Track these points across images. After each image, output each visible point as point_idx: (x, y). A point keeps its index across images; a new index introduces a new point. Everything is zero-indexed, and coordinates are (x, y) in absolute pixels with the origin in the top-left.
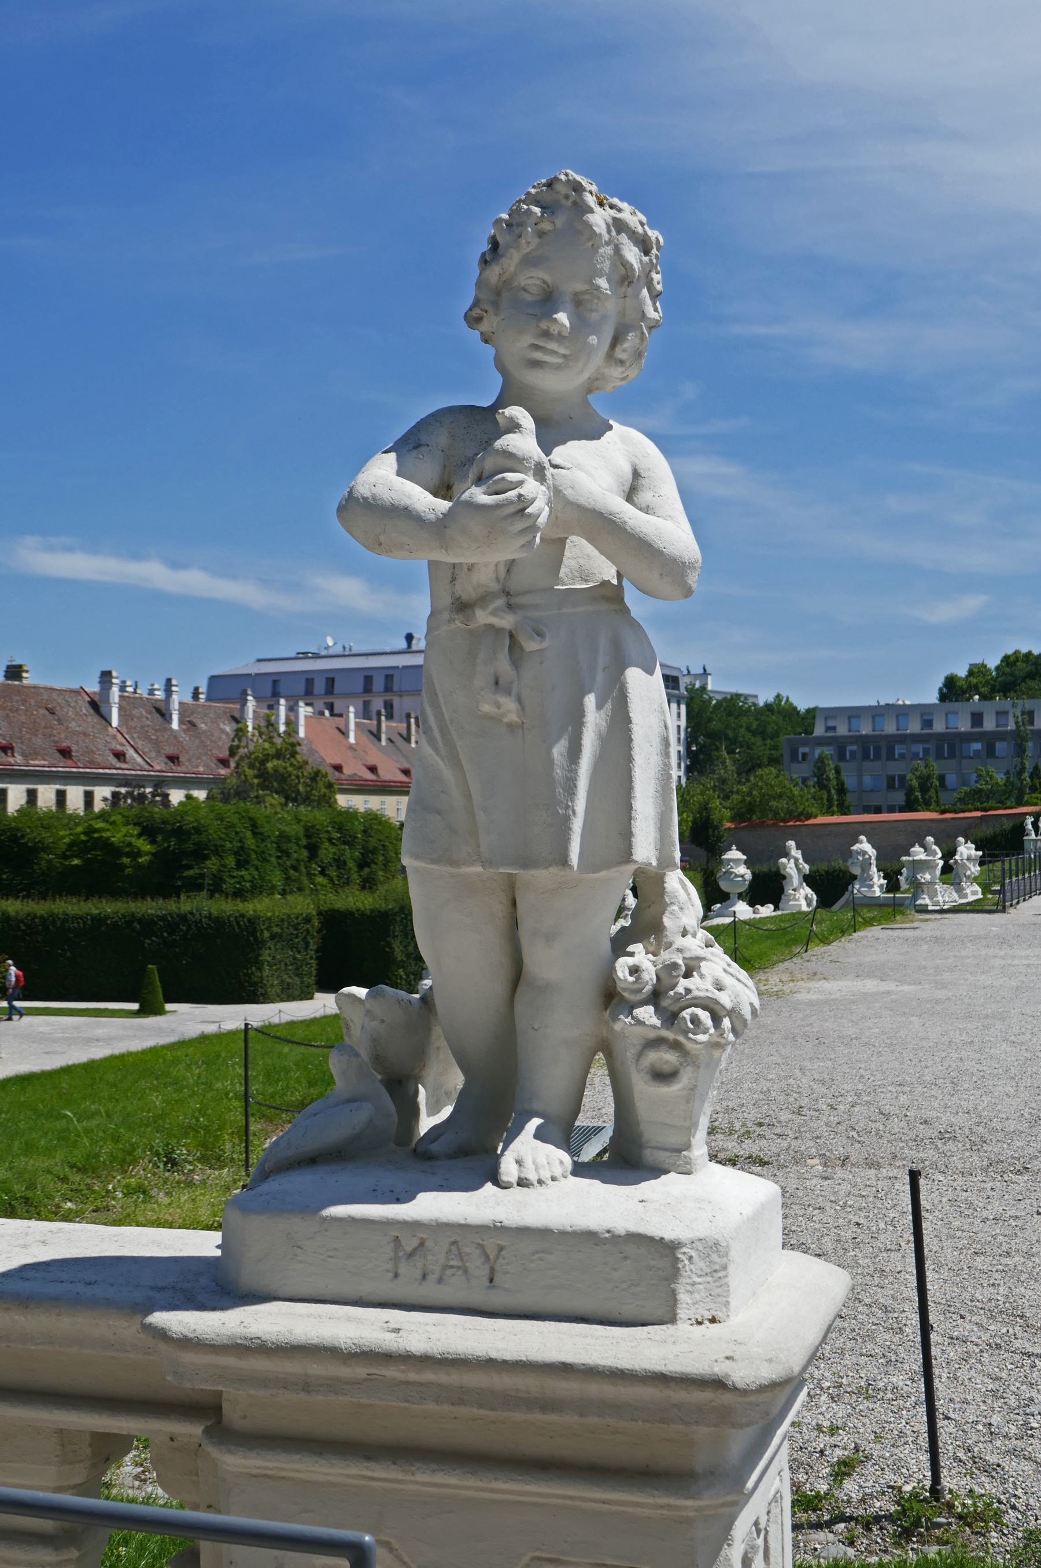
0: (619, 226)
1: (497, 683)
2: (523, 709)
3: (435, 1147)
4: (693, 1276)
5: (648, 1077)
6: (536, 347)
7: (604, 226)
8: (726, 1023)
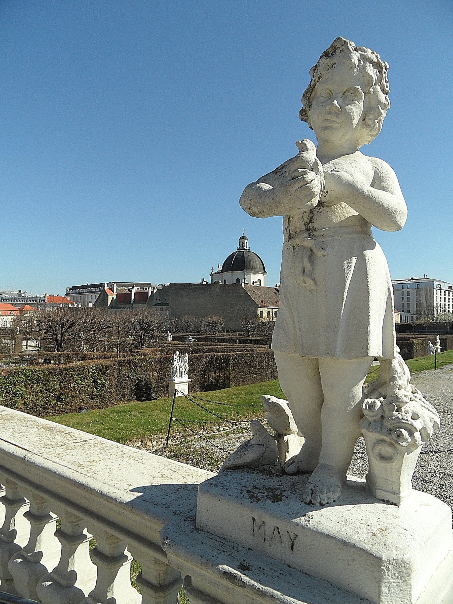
0: (365, 59)
1: (304, 272)
2: (316, 283)
3: (288, 469)
4: (390, 578)
5: (378, 458)
6: (327, 120)
7: (357, 59)
8: (417, 435)
